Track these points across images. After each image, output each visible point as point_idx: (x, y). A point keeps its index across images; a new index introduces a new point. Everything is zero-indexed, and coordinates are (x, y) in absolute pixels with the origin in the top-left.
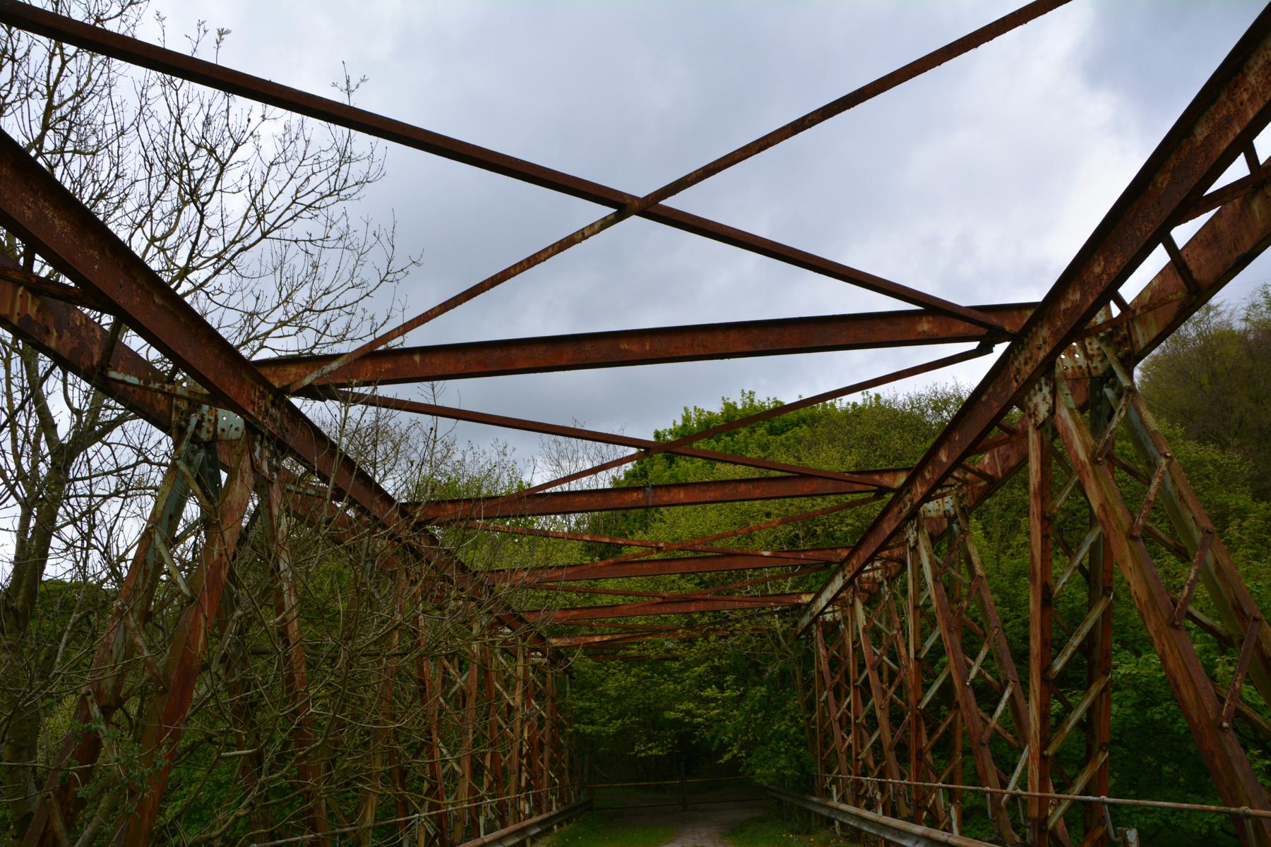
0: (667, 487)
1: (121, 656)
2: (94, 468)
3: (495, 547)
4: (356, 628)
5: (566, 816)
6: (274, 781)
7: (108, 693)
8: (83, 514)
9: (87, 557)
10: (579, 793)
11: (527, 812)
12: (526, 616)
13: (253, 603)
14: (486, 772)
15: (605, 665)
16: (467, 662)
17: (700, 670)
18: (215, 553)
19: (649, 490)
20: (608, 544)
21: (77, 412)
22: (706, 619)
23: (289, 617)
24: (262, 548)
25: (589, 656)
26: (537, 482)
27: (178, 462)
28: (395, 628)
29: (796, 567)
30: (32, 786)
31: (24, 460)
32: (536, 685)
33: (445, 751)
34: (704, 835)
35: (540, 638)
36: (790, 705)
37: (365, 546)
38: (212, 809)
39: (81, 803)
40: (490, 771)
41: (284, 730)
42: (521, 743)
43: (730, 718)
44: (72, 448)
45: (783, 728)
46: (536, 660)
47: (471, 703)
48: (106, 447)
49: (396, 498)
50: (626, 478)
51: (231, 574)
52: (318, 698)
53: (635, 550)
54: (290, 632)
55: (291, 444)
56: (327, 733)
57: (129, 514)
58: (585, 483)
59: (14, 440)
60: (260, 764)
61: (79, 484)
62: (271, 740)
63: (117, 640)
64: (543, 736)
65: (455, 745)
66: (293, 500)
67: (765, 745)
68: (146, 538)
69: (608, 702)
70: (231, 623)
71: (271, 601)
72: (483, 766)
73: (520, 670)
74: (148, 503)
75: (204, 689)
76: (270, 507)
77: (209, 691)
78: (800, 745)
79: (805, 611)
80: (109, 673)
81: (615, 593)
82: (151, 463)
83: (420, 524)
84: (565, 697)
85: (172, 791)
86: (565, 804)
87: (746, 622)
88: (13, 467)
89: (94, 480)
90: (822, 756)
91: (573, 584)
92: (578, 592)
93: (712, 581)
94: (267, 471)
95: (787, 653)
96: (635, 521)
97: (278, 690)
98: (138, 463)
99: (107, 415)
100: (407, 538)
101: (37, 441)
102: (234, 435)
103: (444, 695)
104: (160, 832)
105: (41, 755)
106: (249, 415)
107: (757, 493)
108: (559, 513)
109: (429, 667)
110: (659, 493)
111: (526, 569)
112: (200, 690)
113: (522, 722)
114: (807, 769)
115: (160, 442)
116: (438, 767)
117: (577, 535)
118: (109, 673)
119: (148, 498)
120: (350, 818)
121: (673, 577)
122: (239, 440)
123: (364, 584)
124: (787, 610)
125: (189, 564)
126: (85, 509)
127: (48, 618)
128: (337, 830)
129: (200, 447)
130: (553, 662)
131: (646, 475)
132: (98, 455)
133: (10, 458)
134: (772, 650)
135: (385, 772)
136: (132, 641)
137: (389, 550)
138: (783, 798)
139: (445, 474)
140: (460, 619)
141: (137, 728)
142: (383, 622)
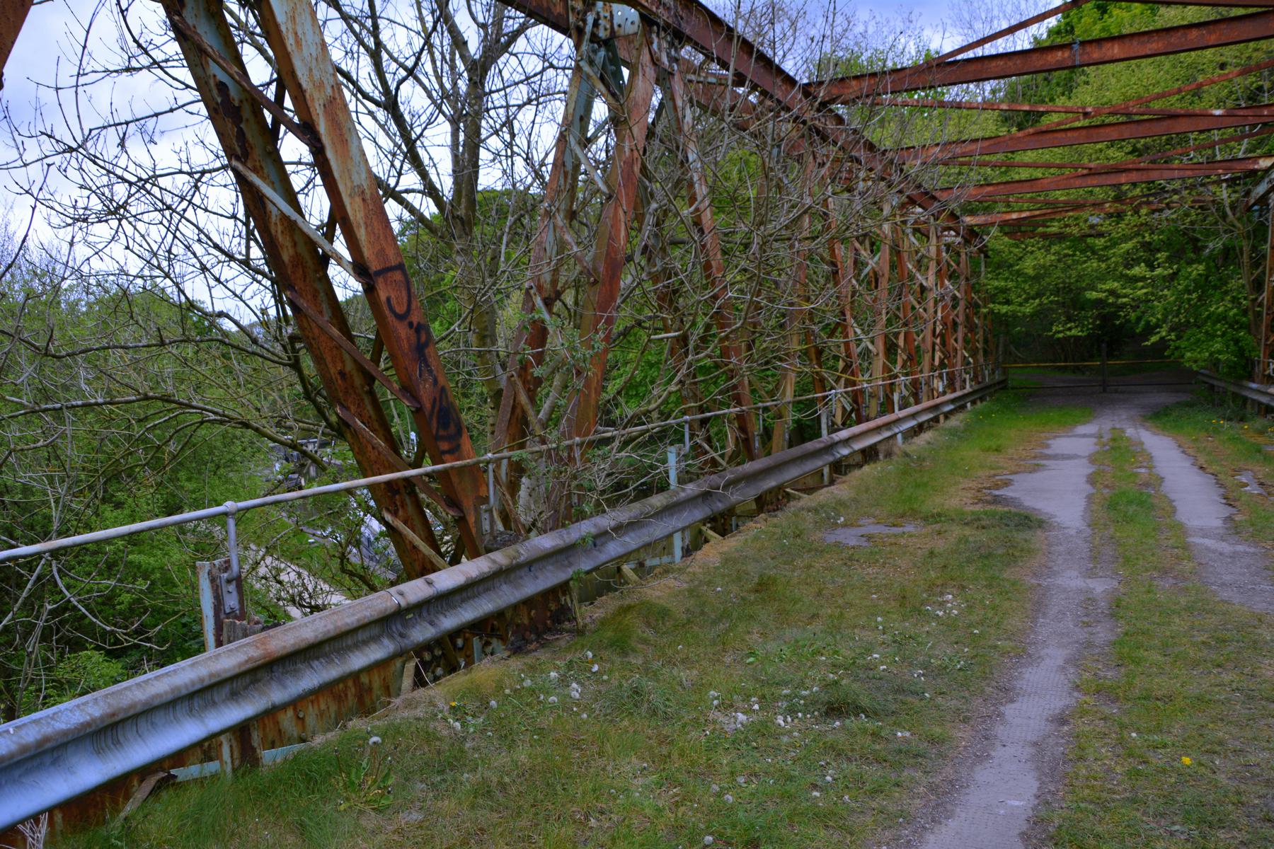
0: (1099, 41)
1: (554, 252)
2: (505, 79)
3: (903, 124)
4: (767, 213)
5: (980, 394)
6: (698, 361)
7: (547, 286)
8: (503, 125)
9: (513, 164)
10: (993, 373)
11: (941, 389)
12: (937, 194)
13: (667, 195)
14: (899, 351)
15: (1022, 243)
16: (878, 243)
17: (1128, 246)
18: (627, 149)
19: (1076, 47)
20: (1027, 113)
21: (483, 26)
22: (1137, 191)
23: (702, 207)
24: (670, 140)
25: (1006, 234)
26: (947, 49)
27: (582, 64)
28: (805, 212)
29: (1255, 126)
30: (498, 368)
31: (445, 80)
32: (949, 264)
33: (859, 331)
34: (1124, 417)
35: (953, 216)
36: (1232, 284)
37: (770, 131)
38: (646, 386)
39: (538, 381)
40: (903, 350)
41: (705, 315)
42: (935, 323)
43: (1159, 299)
44: (484, 62)
45: (1220, 309)
46: (949, 240)
47: (884, 284)
48: (513, 58)
49: (797, 78)
50: (1049, 36)
51: (644, 169)
52: (734, 284)
53: (1055, 118)
54: (704, 222)
55: (687, 31)
56: (746, 315)
57: (544, 120)
58: (1001, 46)
59: (433, 61)
60: (686, 345)
61: (495, 96)
62: (694, 324)
63: (549, 238)
64: (957, 316)
65: (869, 326)
66: (695, 90)
67: (1199, 327)
68: (562, 140)
69: (1025, 282)
70: (648, 216)
71: (684, 192)
72: (897, 346)
73: (933, 250)
74: (558, 108)
75: (629, 279)
76: (673, 99)
77: (634, 280)
78: (1241, 327)
79: (1262, 178)
80: (546, 269)
81: (1035, 166)
82: (556, 68)
83: (824, 105)
84: (979, 276)
85: (610, 371)
86: (979, 383)
87: (1185, 193)
88: (437, 87)
89: (508, 90)
90: (1267, 339)
91: (987, 158)
92: (994, 166)
93: (1147, 147)
94: (666, 62)
95: (1234, 226)
96: (1058, 84)
97: (696, 278)
98: (544, 70)
99: (511, 25)
100: (812, 119)
101: (453, 60)
102: (630, 29)
103: (857, 277)
104: (605, 405)
105: (501, 343)
106: (643, 7)
107: (1213, 39)
108: (972, 82)
109: (840, 250)
110: (1088, 49)
111: (937, 145)
112: (626, 280)
113: (936, 303)
114: (1247, 354)
115: (561, 46)
116: (853, 345)
117: (993, 104)
118: (546, 269)
119: (558, 102)
120: (771, 394)
121: (1099, 146)
122: (636, 34)
123: (772, 169)
124: (1239, 178)
125: (604, 163)
126: (504, 119)
127: (488, 224)
128: (760, 404)
129: (600, 46)
130: (967, 242)
131: (1072, 31)
132: (508, 67)
133: (433, 79)
134: (1216, 223)
135: (801, 351)
136: (561, 238)
137: (794, 133)
138: (1215, 383)
139: (846, 49)
140: (871, 199)
141: (576, 317)
142: (793, 207)
